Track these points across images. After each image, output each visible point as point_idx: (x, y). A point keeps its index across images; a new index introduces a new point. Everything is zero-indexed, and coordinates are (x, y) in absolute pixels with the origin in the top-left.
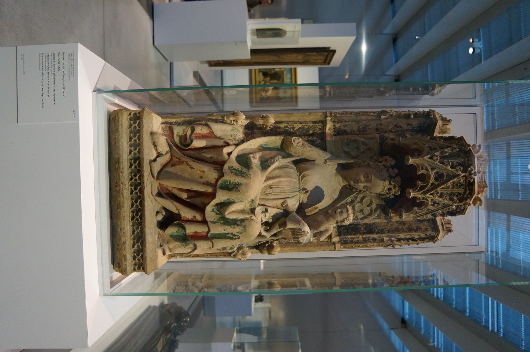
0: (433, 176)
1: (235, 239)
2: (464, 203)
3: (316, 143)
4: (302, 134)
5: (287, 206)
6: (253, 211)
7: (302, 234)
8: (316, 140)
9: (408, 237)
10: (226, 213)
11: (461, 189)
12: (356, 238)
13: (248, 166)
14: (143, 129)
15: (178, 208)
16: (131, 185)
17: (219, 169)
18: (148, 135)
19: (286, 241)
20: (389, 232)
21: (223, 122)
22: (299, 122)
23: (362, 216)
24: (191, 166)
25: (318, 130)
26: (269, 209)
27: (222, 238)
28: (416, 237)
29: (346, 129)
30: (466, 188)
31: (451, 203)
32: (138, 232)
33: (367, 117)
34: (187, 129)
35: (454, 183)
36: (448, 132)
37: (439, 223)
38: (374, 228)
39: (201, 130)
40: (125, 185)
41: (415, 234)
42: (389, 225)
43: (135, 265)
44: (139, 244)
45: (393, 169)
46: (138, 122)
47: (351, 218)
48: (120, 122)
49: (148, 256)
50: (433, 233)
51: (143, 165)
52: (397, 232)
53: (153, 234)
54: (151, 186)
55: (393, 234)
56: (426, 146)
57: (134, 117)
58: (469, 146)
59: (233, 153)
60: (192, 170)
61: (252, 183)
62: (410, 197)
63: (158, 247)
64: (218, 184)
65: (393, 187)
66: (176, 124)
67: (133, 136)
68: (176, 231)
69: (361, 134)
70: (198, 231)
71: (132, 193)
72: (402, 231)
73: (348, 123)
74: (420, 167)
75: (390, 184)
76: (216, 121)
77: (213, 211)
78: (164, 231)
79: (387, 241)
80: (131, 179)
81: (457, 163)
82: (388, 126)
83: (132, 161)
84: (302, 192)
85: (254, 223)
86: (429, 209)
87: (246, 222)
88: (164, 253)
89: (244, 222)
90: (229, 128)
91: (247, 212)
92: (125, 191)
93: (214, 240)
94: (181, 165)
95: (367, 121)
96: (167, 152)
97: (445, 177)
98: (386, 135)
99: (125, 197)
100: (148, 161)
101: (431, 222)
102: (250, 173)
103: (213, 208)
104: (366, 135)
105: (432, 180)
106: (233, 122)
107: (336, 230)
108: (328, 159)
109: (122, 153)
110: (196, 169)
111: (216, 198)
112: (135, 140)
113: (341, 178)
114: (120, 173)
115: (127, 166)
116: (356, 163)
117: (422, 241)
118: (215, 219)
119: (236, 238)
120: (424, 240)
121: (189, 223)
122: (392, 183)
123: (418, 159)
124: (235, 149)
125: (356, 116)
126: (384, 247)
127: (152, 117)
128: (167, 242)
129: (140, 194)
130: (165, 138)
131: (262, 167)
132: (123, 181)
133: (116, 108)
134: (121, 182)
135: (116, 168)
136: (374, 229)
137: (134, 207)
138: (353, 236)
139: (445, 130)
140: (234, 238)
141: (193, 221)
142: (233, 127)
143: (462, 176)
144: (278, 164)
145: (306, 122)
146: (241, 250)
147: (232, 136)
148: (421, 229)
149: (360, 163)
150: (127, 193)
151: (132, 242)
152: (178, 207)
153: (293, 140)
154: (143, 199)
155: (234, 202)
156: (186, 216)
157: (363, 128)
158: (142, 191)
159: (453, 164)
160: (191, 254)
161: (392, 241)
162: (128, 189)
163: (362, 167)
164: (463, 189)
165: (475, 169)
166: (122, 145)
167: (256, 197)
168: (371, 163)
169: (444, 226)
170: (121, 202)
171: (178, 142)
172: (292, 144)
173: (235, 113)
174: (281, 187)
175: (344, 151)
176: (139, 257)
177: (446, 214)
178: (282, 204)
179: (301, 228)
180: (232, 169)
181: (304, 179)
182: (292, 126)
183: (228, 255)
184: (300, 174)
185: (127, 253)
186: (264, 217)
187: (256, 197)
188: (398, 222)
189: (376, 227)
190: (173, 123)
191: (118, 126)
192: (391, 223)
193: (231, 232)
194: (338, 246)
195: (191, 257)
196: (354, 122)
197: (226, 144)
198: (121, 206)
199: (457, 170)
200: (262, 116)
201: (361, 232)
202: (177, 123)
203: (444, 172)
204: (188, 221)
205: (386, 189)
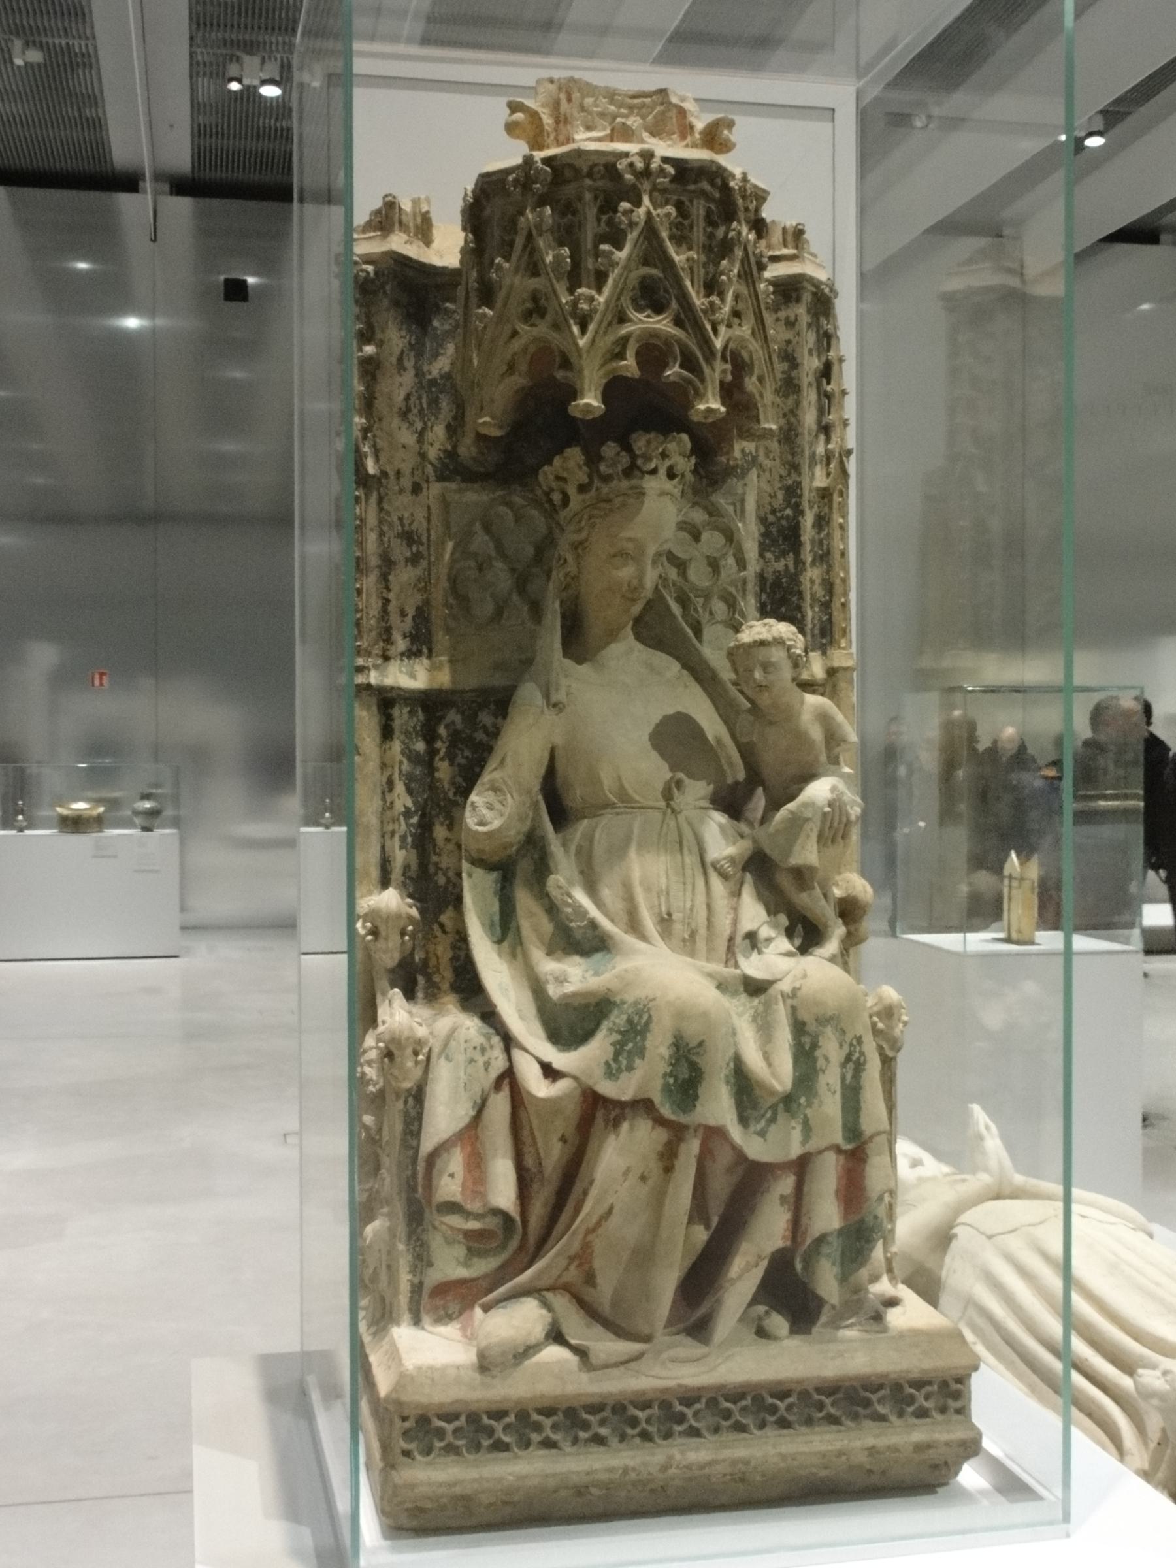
0: (648, 316)
1: (862, 1053)
3: (459, 725)
4: (429, 780)
5: (732, 860)
6: (755, 988)
8: (447, 726)
11: (694, 211)
13: (598, 1004)
14: (466, 1403)
16: (668, 1435)
18: (488, 1380)
20: (795, 467)
21: (418, 1095)
22: (383, 793)
25: (415, 719)
26: (747, 925)
27: (858, 1102)
29: (411, 612)
32: (833, 1404)
33: (372, 530)
34: (444, 1227)
36: (425, 208)
38: (779, 519)
39: (452, 1176)
42: (767, 463)
43: (943, 1410)
44: (874, 1398)
50: (807, 297)
52: (797, 436)
53: (841, 1347)
55: (803, 451)
58: (528, 161)
60: (614, 1211)
62: (723, 409)
64: (673, 1117)
67: (490, 1437)
69: (429, 549)
71: (694, 1433)
72: (795, 416)
75: (654, 472)
76: (414, 1123)
77: (762, 1134)
80: (645, 1436)
81: (599, 220)
83: (583, 1435)
84: (679, 799)
87: (803, 1015)
89: (804, 1024)
91: (761, 1008)
94: (593, 1252)
95: (385, 528)
96: (545, 1304)
98: (433, 453)
100: (585, 1377)
104: (432, 533)
105: (661, 324)
108: (547, 696)
111: (724, 1126)
112: (507, 1428)
113: (613, 646)
117: (833, 342)
119: (858, 1049)
121: (804, 1220)
122: (653, 466)
123: (586, 373)
125: (367, 571)
130: (478, 1311)
131: (597, 950)
132: (658, 1467)
136: (784, 522)
137: (744, 1421)
139: (419, 220)
140: (858, 1059)
141: (798, 1203)
143: (651, 208)
145: (383, 766)
147: (472, 1061)
148: (789, 342)
151: (868, 1423)
153: (481, 829)
154: (720, 1388)
157: (409, 546)
158: (690, 1397)
159: (603, 239)
164: (695, 202)
165: (626, 155)
169: (777, 253)
170: (729, 1470)
171: (491, 1259)
172: (499, 830)
173: (387, 1047)
174: (663, 881)
178: (724, 876)
180: (614, 1065)
181: (630, 791)
182: (402, 818)
184: (611, 805)
189: (773, 512)
190: (416, 1281)
193: (839, 1070)
197: (506, 1081)
198: (744, 1468)
199: (632, 224)
202: (416, 1267)
204: (796, 1226)
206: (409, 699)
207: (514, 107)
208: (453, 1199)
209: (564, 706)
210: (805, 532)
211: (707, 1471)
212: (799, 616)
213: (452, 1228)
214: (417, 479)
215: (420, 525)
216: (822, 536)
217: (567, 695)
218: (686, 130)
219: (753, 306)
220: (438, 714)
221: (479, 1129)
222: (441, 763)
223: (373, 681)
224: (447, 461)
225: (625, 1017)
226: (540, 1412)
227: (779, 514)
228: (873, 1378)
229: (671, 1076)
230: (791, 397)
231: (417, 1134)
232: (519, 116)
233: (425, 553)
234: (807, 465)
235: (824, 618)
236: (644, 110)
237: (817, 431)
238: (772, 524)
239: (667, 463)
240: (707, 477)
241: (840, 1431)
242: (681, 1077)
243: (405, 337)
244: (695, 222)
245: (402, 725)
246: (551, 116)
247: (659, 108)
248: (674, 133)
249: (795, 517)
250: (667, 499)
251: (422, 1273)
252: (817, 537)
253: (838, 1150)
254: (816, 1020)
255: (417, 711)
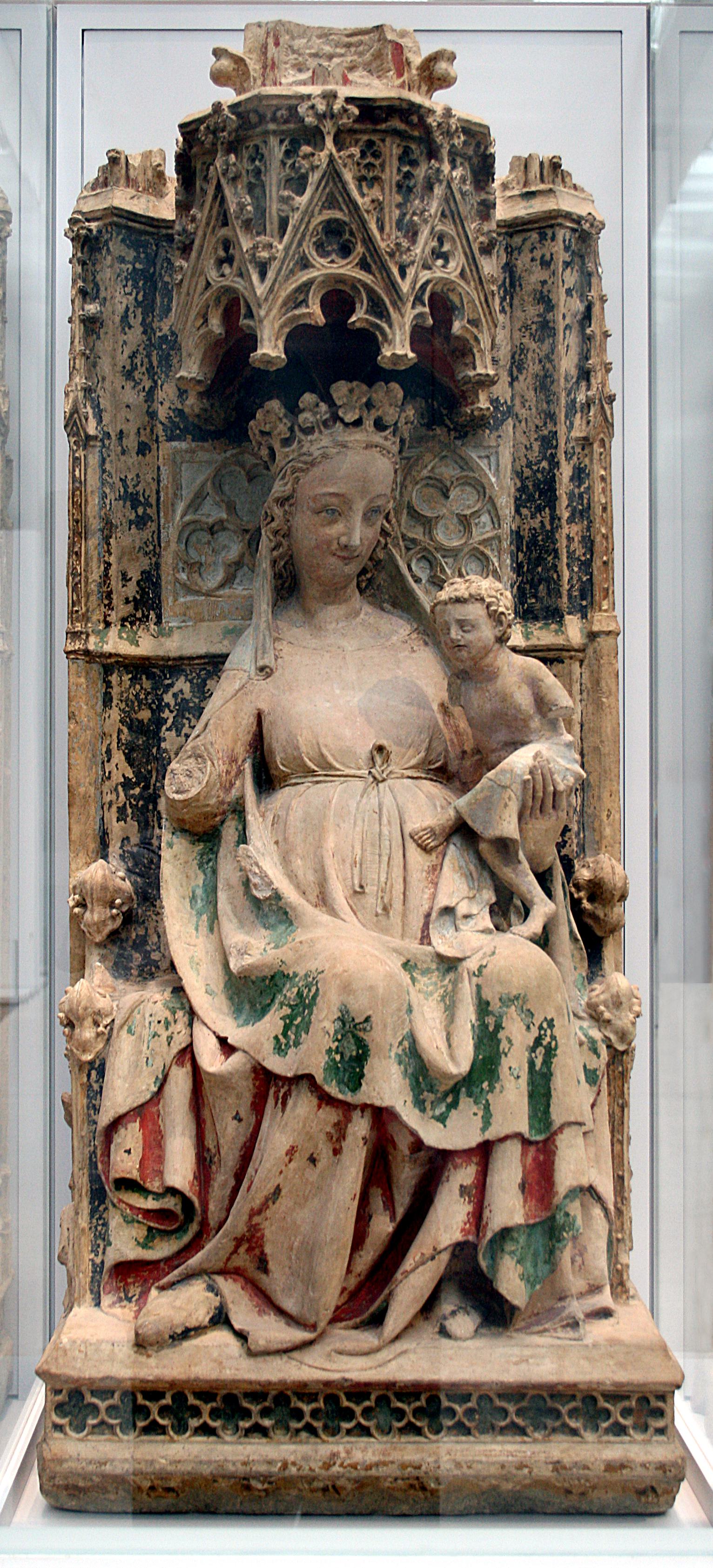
0: (332, 262)
1: (553, 1038)
2: (439, 139)
3: (188, 695)
7: (544, 780)
8: (175, 695)
9: (573, 339)
10: (453, 1070)
12: (572, 548)
15: (428, 1252)
16: (334, 1432)
17: (282, 1091)
18: (143, 1359)
19: (575, 827)
20: (551, 417)
22: (103, 763)
23: (485, 518)
24: (267, 1199)
26: (443, 901)
28: (578, 306)
29: (135, 575)
30: (384, 132)
31: (438, 190)
35: (361, 179)
36: (157, 160)
37: (522, 210)
38: (535, 472)
39: (128, 1152)
40: (334, 1455)
41: (562, 310)
42: (523, 413)
45: (302, 411)
46: (90, 1399)
47: (485, 585)
48: (91, 1468)
49: (610, 1375)
51: (259, 1383)
52: (552, 382)
53: (527, 1352)
54: (340, 1353)
56: (213, 274)
57: (70, 1413)
59: (222, 1035)
60: (283, 1193)
61: (339, 969)
62: (411, 355)
63: (576, 1335)
64: (340, 1096)
65: (373, 411)
66: (100, 1250)
68: (518, 1262)
69: (158, 512)
70: (519, 1180)
72: (551, 361)
73: (114, 567)
74: (297, 312)
77: (442, 1119)
78: (513, 1309)
79: (588, 422)
82: (128, 406)
85: (495, 965)
86: (462, 274)
87: (487, 994)
88: (605, 1313)
89: (488, 1003)
90: (125, 1044)
91: (450, 987)
92: (358, 1456)
93: (554, 1116)
94: (263, 1236)
95: (108, 491)
96: (211, 1288)
97: (338, 215)
98: (163, 413)
99: (382, 1458)
101: (517, 240)
102: (302, 973)
103: (433, 1117)
104: (162, 494)
105: (346, 268)
106: (101, 1029)
107: (538, 625)
109: (209, 1462)
110: (279, 1180)
112: (163, 1411)
114: (287, 1473)
115: (260, 1447)
116: (273, 549)
117: (594, 280)
118: (475, 1114)
119: (549, 1032)
120: (590, 275)
121: (486, 1213)
124: (209, 1024)
126: (611, 435)
127: (74, 1342)
128: (561, 1299)
129: (369, 1399)
132: (320, 1464)
133: (34, 1481)
134: (323, 1472)
135: (266, 1490)
136: (539, 476)
137: (418, 1424)
138: (565, 560)
139: (150, 173)
140: (550, 1043)
142: (121, 1027)
143: (334, 151)
144: (268, 859)
146: (602, 1013)
148: (544, 283)
149: (276, 533)
150: (364, 1450)
151: (561, 1437)
152: (422, 1254)
154: (390, 1386)
155: (412, 1039)
156: (461, 1225)
157: (134, 507)
160: (611, 1207)
161: (588, 404)
162: (349, 1446)
163: (289, 529)
164: (387, 143)
165: (309, 97)
166: (179, 1461)
167: (395, 950)
168: (279, 488)
170: (398, 1473)
172: (196, 798)
173: (67, 1017)
175: (222, 586)
176: (615, 1410)
177: (483, 196)
178: (426, 850)
179: (519, 781)
180: (283, 1040)
181: (331, 759)
182: (120, 789)
183: (621, 1062)
185: (596, 1454)
186: (472, 922)
187: (395, 950)
188: (515, 373)
189: (529, 465)
190: (98, 1260)
191: (104, 1476)
192: (517, 402)
193: (527, 1054)
194: (599, 622)
195: (624, 1208)
196: (109, 544)
198: (415, 1473)
200: (76, 910)
201: (548, 527)
203: (320, 219)
204: (478, 1217)
205: (378, 438)
206: (132, 665)
207: (218, 53)
208: (128, 1176)
209: (272, 670)
210: (560, 484)
211: (373, 1472)
212: (555, 576)
213: (132, 1207)
214: (143, 438)
215: (148, 487)
216: (582, 490)
217: (276, 659)
218: (401, 65)
219: (463, 247)
220: (167, 682)
221: (160, 1106)
222: (167, 733)
223: (91, 647)
224: (177, 420)
225: (295, 990)
226: (198, 1395)
227: (535, 468)
228: (560, 1387)
229: (337, 1053)
230: (547, 342)
231: (97, 1110)
232: (225, 63)
233: (155, 517)
234: (563, 414)
235: (584, 579)
236: (361, 48)
237: (578, 378)
238: (527, 478)
239: (374, 414)
240: (455, 429)
241: (525, 1442)
242: (347, 1055)
243: (130, 294)
244: (387, 160)
245: (122, 693)
246: (259, 61)
247: (376, 46)
248: (389, 71)
249: (551, 470)
250: (375, 452)
251: (104, 1253)
252: (576, 491)
253: (526, 1142)
254: (500, 999)
255: (141, 679)
